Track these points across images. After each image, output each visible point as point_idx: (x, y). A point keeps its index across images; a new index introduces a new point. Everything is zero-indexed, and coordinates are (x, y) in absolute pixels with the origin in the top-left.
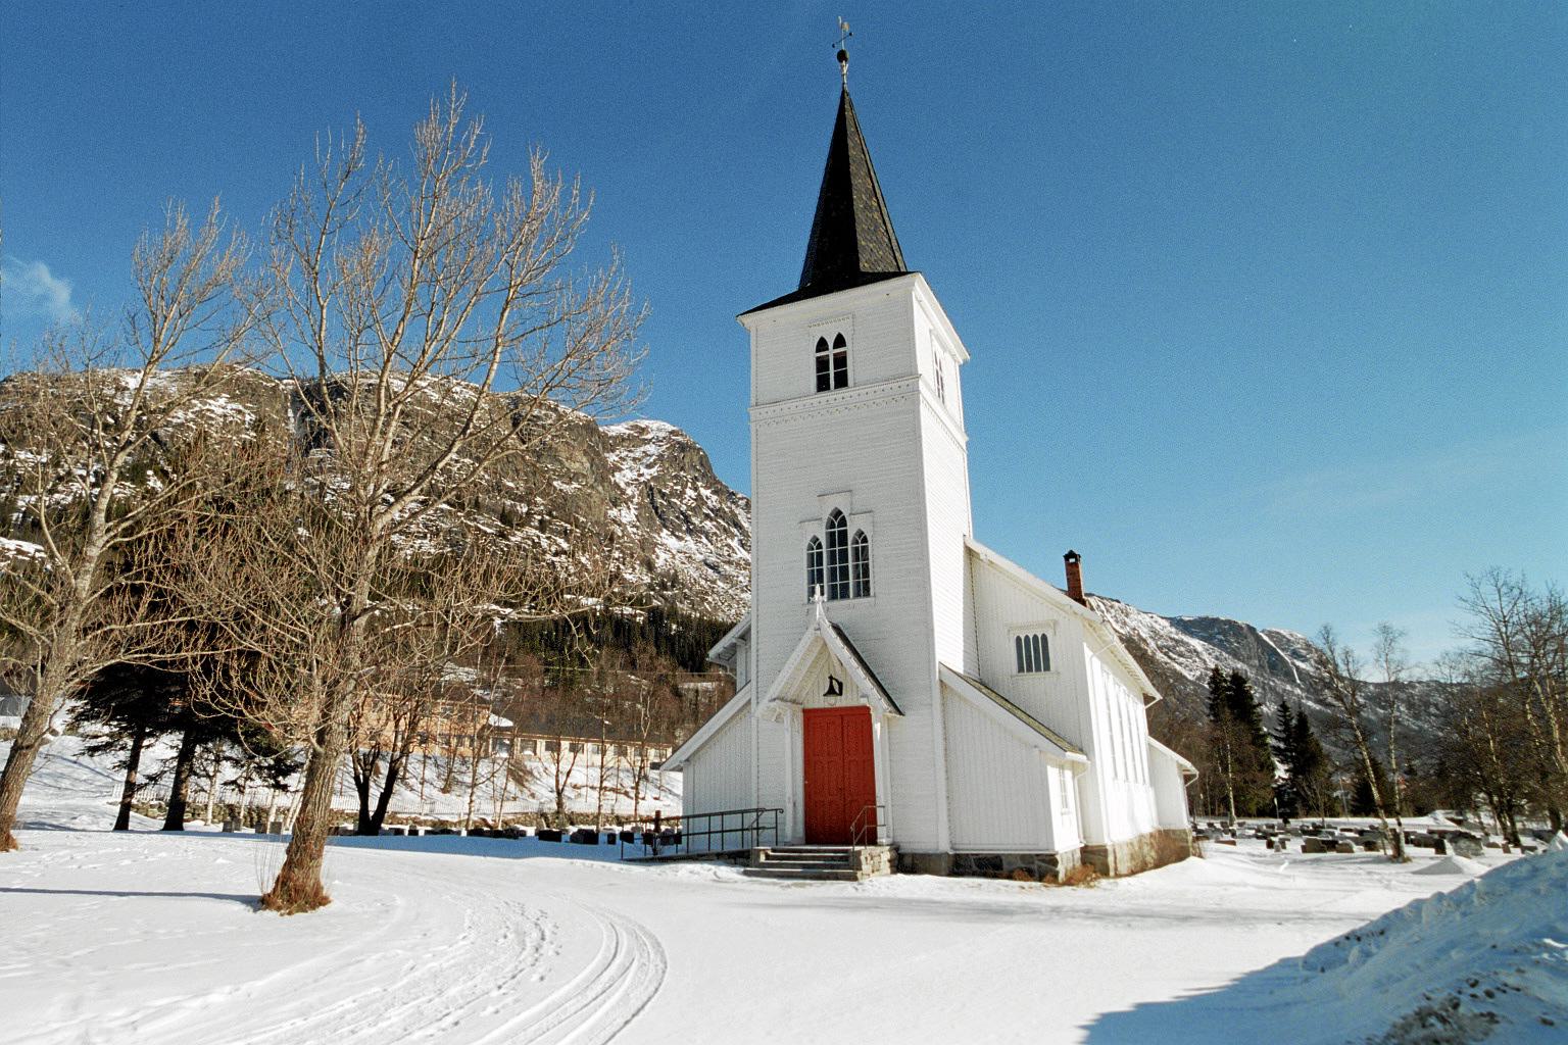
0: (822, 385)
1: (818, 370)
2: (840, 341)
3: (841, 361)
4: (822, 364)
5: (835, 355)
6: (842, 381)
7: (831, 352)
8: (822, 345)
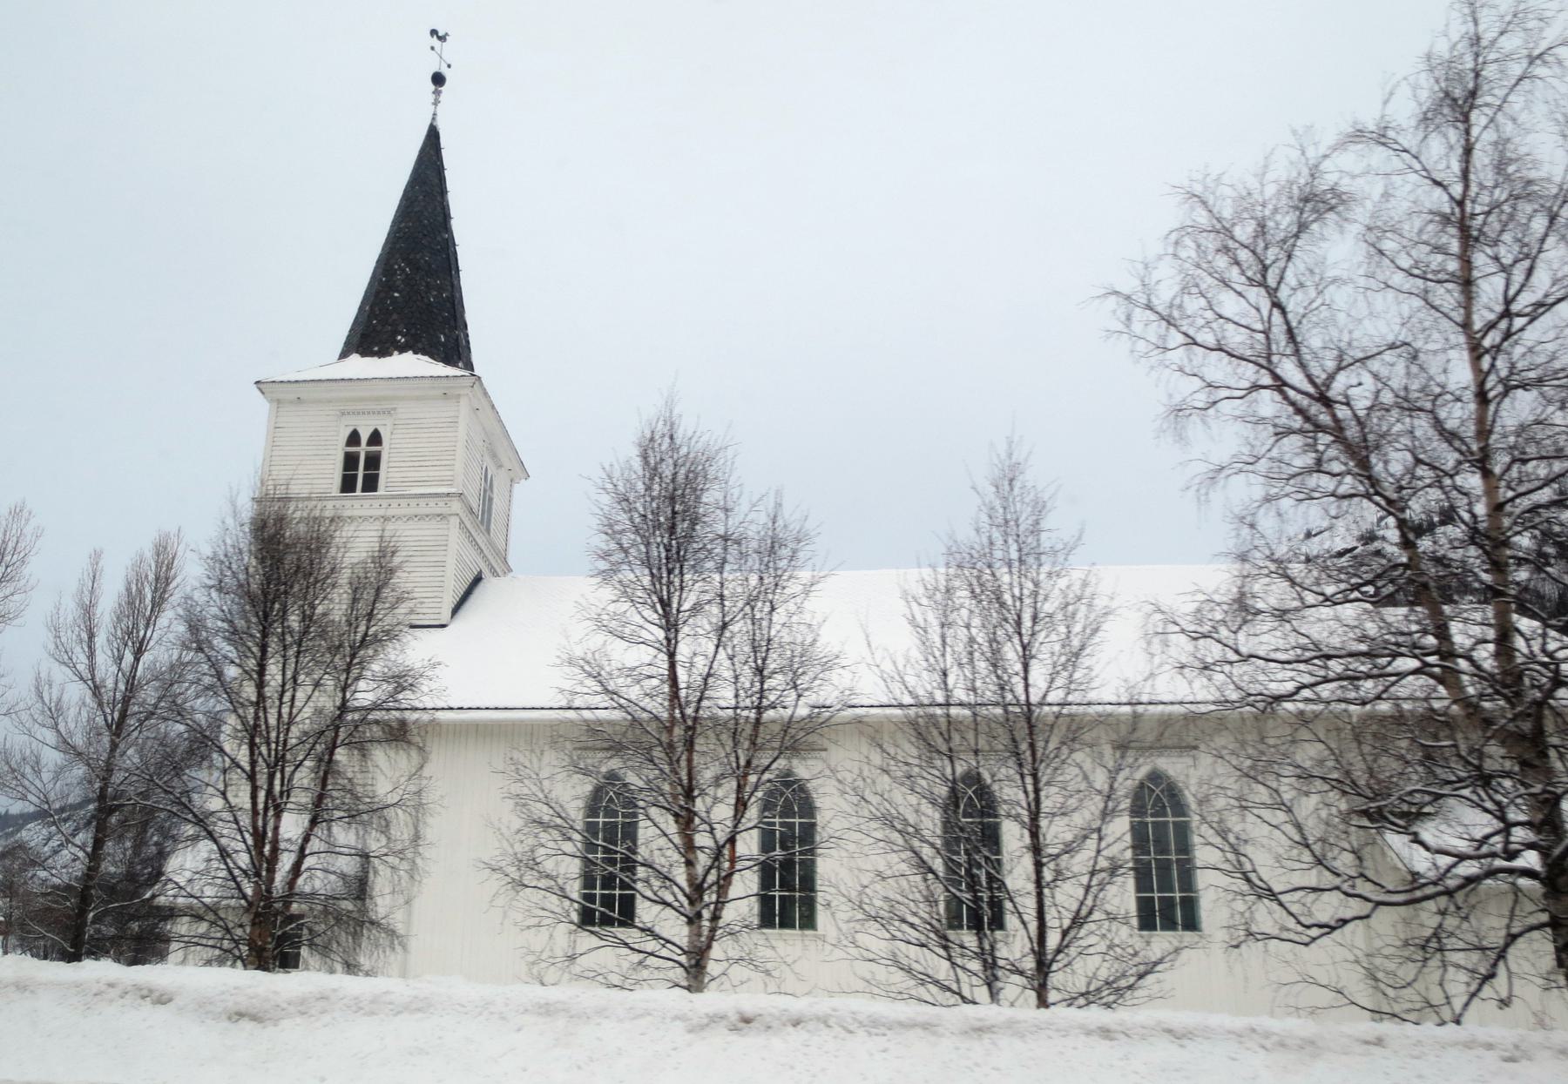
0: (348, 485)
1: (346, 469)
2: (375, 438)
3: (373, 462)
4: (350, 461)
5: (367, 454)
6: (371, 484)
7: (363, 450)
8: (354, 438)
